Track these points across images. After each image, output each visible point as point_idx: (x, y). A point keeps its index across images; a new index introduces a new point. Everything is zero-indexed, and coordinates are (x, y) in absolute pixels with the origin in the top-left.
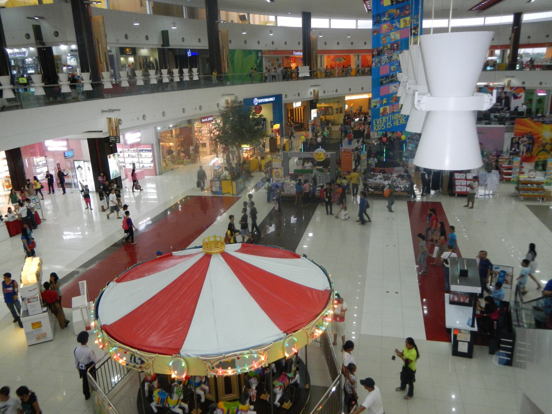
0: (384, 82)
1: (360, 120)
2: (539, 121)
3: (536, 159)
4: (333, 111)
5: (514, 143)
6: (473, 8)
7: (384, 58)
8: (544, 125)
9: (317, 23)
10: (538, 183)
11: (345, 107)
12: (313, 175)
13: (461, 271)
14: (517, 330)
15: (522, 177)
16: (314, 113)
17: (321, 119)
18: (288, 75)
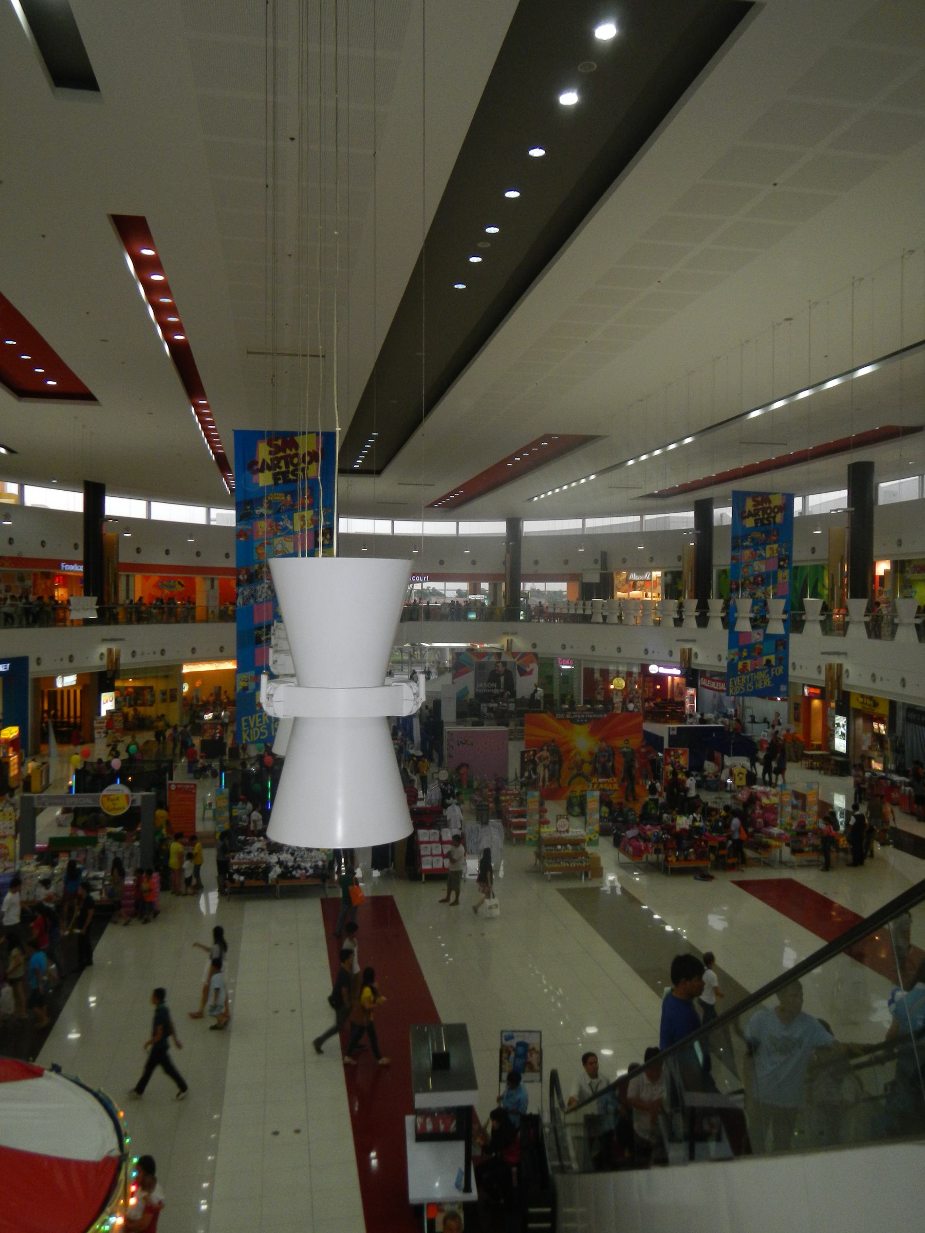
1: (215, 717)
2: (565, 719)
3: (568, 794)
4: (153, 695)
5: (528, 763)
6: (436, 502)
8: (577, 727)
9: (116, 506)
10: (576, 843)
11: (182, 688)
12: (98, 848)
13: (435, 1056)
14: (559, 1180)
15: (547, 831)
16: (107, 703)
17: (125, 716)
18: (44, 614)
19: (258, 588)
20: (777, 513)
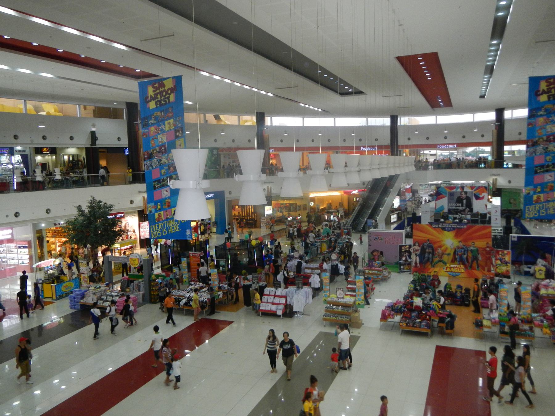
0: (539, 171)
2: (438, 227)
7: (155, 161)
8: (446, 232)
19: (537, 148)
20: (170, 94)
